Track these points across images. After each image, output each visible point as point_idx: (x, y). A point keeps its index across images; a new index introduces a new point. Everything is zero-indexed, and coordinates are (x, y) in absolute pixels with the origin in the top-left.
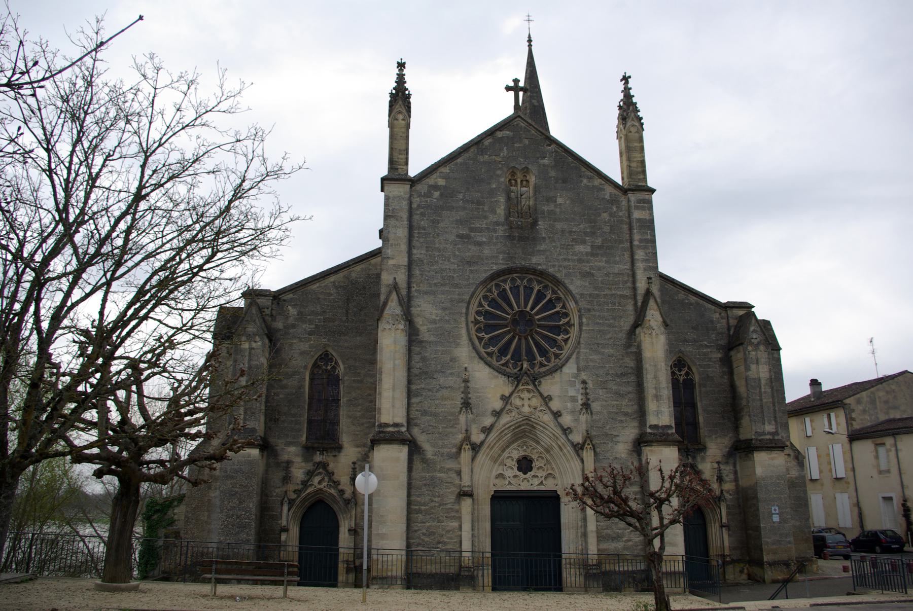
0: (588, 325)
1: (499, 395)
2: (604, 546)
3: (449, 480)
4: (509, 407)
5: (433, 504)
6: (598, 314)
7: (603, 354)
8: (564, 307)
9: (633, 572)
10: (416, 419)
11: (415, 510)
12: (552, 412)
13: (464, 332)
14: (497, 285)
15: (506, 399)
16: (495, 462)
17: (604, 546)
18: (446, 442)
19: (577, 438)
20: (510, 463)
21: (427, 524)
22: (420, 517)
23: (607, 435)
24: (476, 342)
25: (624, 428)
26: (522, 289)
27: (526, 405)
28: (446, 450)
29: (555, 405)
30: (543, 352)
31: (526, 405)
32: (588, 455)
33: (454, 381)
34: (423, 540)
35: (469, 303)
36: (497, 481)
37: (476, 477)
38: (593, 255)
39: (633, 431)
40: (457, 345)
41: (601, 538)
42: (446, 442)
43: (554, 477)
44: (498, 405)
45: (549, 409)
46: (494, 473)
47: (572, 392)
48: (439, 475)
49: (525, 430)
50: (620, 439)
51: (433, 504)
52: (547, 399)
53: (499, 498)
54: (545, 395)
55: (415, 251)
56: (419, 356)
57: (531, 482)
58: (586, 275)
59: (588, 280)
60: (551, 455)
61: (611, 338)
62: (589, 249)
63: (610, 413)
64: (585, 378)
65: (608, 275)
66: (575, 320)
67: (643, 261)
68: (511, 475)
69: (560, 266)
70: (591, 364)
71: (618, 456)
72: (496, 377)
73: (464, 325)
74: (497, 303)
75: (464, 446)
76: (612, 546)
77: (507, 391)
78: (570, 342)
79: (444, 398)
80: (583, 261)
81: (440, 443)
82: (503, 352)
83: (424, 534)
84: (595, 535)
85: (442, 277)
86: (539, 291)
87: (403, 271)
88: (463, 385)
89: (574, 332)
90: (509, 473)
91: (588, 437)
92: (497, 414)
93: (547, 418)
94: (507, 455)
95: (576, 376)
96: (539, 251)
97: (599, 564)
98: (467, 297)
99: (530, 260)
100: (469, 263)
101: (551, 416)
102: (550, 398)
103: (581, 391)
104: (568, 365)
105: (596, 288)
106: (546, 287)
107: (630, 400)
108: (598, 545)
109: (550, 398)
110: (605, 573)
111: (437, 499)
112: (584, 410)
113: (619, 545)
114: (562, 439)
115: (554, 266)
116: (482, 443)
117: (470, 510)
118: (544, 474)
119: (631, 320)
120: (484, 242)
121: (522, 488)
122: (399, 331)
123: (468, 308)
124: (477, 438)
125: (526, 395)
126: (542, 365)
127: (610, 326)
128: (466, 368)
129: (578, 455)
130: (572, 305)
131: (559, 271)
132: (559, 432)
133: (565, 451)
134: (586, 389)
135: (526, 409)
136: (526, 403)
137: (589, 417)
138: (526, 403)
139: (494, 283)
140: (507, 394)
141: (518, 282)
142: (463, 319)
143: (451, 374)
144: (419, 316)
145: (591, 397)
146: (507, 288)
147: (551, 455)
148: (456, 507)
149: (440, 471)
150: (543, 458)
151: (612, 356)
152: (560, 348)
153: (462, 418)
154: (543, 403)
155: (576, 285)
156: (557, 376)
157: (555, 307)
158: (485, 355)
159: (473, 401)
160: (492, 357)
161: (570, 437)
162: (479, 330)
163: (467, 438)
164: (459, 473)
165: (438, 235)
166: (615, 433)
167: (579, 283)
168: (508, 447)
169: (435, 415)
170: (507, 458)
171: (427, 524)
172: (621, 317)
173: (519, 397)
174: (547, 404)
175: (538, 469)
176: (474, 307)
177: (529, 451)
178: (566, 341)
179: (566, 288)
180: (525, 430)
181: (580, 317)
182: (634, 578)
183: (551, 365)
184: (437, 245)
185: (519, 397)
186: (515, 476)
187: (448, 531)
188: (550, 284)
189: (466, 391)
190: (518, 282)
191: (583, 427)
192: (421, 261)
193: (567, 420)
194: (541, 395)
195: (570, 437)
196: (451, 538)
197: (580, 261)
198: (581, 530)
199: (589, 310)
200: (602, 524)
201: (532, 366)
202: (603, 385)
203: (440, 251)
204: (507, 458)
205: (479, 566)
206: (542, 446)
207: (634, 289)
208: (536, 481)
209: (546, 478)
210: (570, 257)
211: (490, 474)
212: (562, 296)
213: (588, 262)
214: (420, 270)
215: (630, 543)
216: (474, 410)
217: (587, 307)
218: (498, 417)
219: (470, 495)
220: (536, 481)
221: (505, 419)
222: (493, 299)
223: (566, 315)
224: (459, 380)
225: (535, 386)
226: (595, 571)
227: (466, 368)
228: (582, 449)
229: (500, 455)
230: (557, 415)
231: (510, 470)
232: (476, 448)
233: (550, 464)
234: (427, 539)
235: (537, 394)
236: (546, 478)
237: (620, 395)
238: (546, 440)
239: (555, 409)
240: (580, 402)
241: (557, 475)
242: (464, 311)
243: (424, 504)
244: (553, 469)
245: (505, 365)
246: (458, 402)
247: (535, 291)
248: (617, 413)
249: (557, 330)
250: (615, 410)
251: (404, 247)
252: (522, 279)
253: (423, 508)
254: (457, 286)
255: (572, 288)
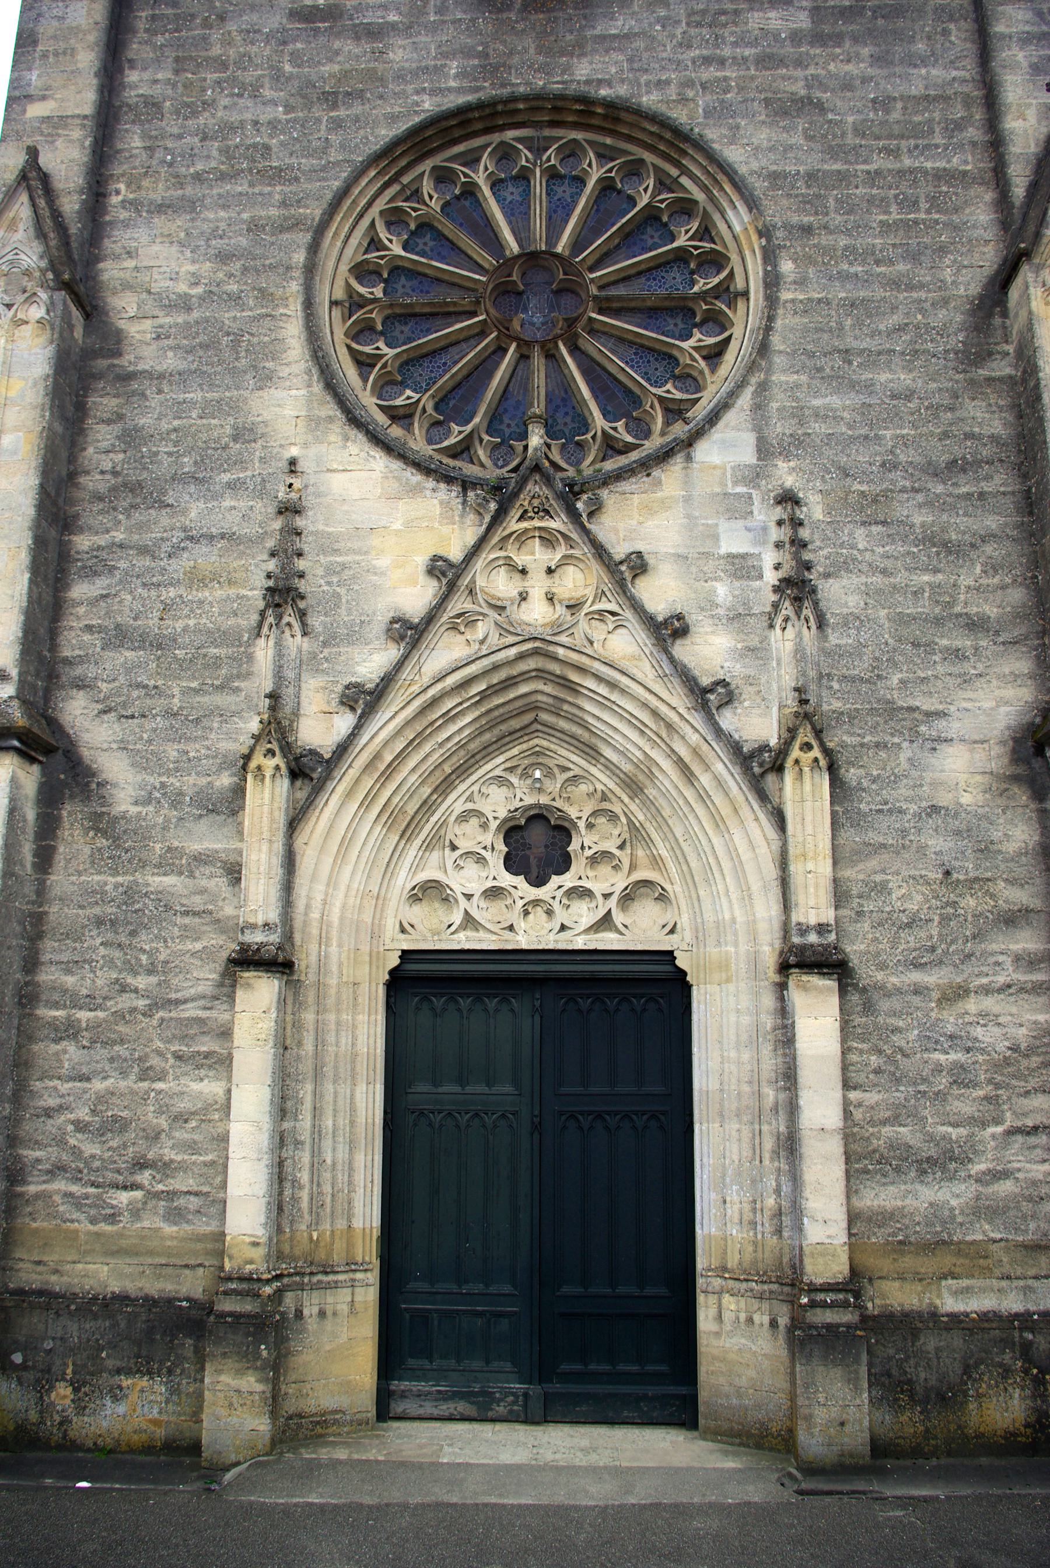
0: (801, 283)
1: (421, 560)
2: (879, 1197)
3: (197, 902)
4: (459, 603)
5: (125, 1002)
6: (843, 241)
7: (869, 387)
8: (706, 232)
9: (1024, 1320)
10: (81, 660)
11: (53, 1025)
12: (649, 621)
13: (293, 332)
14: (443, 177)
15: (447, 574)
16: (407, 834)
17: (879, 1197)
18: (194, 750)
19: (758, 723)
20: (470, 836)
21: (98, 1085)
22: (71, 1053)
23: (891, 710)
24: (351, 372)
25: (966, 681)
26: (538, 184)
27: (537, 594)
28: (191, 783)
29: (660, 593)
30: (620, 400)
31: (537, 594)
32: (805, 795)
33: (248, 514)
34: (76, 1152)
35: (320, 231)
36: (416, 913)
37: (309, 889)
38: (818, 38)
39: (1009, 693)
40: (266, 379)
41: (861, 1161)
42: (194, 750)
43: (663, 898)
44: (416, 596)
45: (637, 607)
46: (404, 880)
47: (734, 540)
48: (157, 881)
49: (528, 701)
50: (953, 727)
51: (125, 1002)
52: (626, 571)
53: (419, 983)
54: (619, 551)
55: (132, 76)
56: (117, 428)
57: (562, 916)
58: (784, 109)
59: (801, 124)
60: (648, 804)
61: (901, 329)
62: (802, 21)
63: (901, 620)
64: (789, 481)
65: (883, 103)
66: (750, 272)
67: (1026, 40)
68: (476, 888)
69: (689, 83)
70: (818, 428)
71: (944, 799)
72: (415, 491)
73: (295, 308)
74: (440, 236)
75: (258, 759)
76: (919, 1198)
77: (456, 538)
78: (729, 356)
79: (197, 579)
80: (782, 62)
81: (172, 751)
82: (454, 403)
83: (80, 1127)
84: (835, 1147)
85: (225, 151)
86: (606, 186)
87: (77, 134)
88: (277, 524)
89: (744, 322)
90: (469, 880)
91: (806, 718)
92: (410, 633)
93: (625, 645)
94: (459, 808)
95: (754, 476)
96: (602, 38)
97: (855, 1283)
98: (314, 212)
99: (567, 69)
100: (331, 99)
101: (642, 636)
102: (639, 565)
103: (775, 534)
104: (718, 434)
105: (834, 152)
106: (634, 170)
107: (992, 568)
108: (850, 1192)
109: (639, 565)
110: (906, 1325)
111: (142, 982)
112: (787, 609)
113: (953, 1195)
114: (693, 731)
115: (660, 84)
116: (343, 749)
117: (267, 1025)
118: (620, 882)
119: (988, 257)
120: (393, 26)
121: (523, 941)
122: (27, 330)
123: (314, 248)
124: (319, 728)
125: (536, 556)
126: (611, 447)
127: (895, 283)
128: (293, 462)
129: (763, 797)
130: (737, 220)
131: (683, 100)
132: (676, 700)
133: (705, 779)
134: (797, 523)
135: (537, 614)
136: (537, 586)
137: (809, 636)
138: (537, 585)
139: (427, 165)
140: (455, 553)
141: (525, 156)
142: (295, 287)
143: (231, 486)
144: (127, 286)
145: (819, 555)
146: (480, 178)
147: (648, 804)
148: (219, 1015)
149: (164, 866)
150: (613, 818)
151: (909, 395)
152: (691, 381)
153: (264, 652)
154: (608, 586)
155: (748, 147)
156: (670, 478)
157: (673, 238)
158: (382, 419)
159: (314, 583)
160: (409, 428)
161: (727, 720)
162: (362, 331)
163: (278, 728)
164: (234, 873)
165: (222, 18)
166: (927, 704)
167: (763, 136)
168: (462, 771)
169: (159, 644)
170: (464, 817)
171: (98, 1085)
172: (942, 250)
173: (510, 564)
174: (621, 586)
175: (594, 861)
176: (342, 251)
177: (554, 786)
178: (714, 355)
179: (712, 157)
180: (528, 701)
181: (770, 256)
182: (1026, 1349)
183: (653, 444)
184: (216, 50)
185: (510, 564)
186: (494, 893)
187: (181, 1118)
188: (649, 157)
189: (288, 547)
190: (525, 156)
191: (783, 678)
192: (153, 105)
193: (710, 651)
194: (600, 551)
195: (727, 720)
196: (192, 1147)
197: (765, 61)
198: (775, 1126)
199: (807, 230)
200: (872, 1097)
201: (576, 449)
202: (872, 510)
203: (224, 66)
204: (464, 817)
205: (295, 1267)
206: (610, 767)
207: (996, 143)
208: (584, 914)
209: (627, 898)
210: (727, 52)
211: (386, 884)
212: (699, 196)
213: (799, 63)
214: (145, 136)
215: (1006, 1187)
216: (316, 621)
217: (795, 219)
218: (414, 644)
219: (279, 964)
220: (584, 914)
221: (444, 653)
222: (425, 226)
223: (716, 261)
224: (263, 509)
225: (574, 515)
226: (829, 1317)
227: (293, 462)
228: (778, 768)
229: (427, 807)
230: (669, 631)
231: (471, 869)
232: (308, 771)
233: (648, 842)
234: (91, 1149)
235: (583, 550)
236: (627, 898)
237: (947, 549)
238: (624, 740)
239: (659, 606)
240: (771, 577)
241: (675, 888)
242: (300, 257)
243: (91, 1002)
244: (656, 862)
245: (463, 450)
246: (254, 592)
247: (591, 184)
248: (938, 621)
249: (682, 313)
250: (924, 607)
251: (87, 60)
252: (538, 150)
253: (83, 1015)
254: (278, 175)
255: (734, 155)
